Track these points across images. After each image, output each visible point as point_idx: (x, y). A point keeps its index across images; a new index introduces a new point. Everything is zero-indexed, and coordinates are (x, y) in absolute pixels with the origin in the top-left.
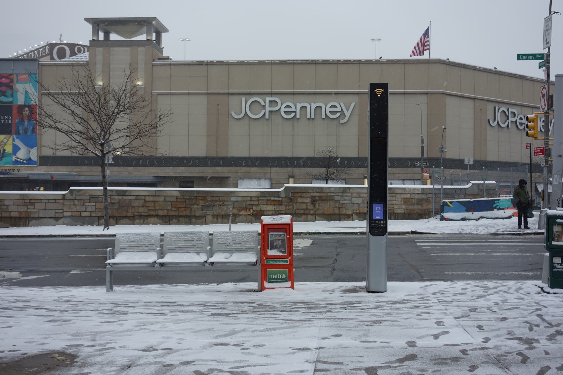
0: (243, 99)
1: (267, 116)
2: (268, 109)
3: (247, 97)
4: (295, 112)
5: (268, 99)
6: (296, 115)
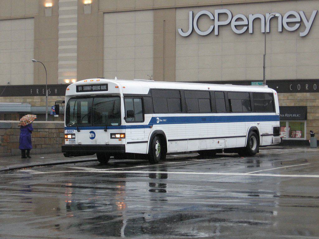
0: (191, 13)
1: (216, 32)
2: (217, 23)
3: (195, 10)
4: (248, 25)
5: (217, 11)
6: (248, 28)
